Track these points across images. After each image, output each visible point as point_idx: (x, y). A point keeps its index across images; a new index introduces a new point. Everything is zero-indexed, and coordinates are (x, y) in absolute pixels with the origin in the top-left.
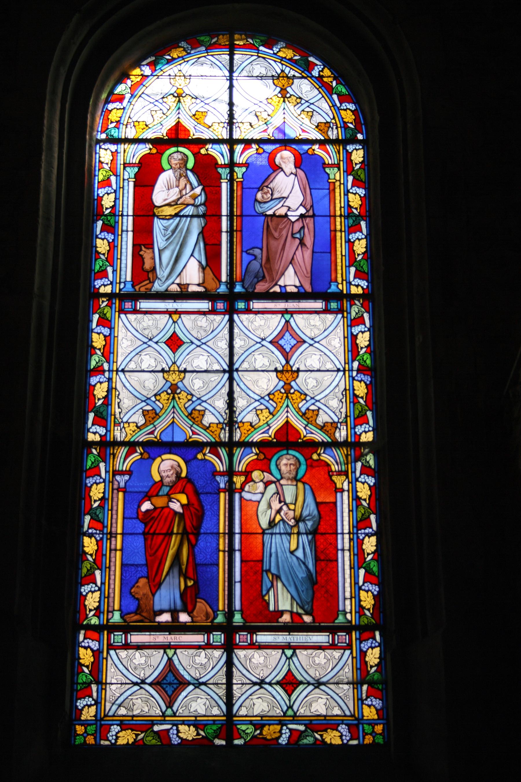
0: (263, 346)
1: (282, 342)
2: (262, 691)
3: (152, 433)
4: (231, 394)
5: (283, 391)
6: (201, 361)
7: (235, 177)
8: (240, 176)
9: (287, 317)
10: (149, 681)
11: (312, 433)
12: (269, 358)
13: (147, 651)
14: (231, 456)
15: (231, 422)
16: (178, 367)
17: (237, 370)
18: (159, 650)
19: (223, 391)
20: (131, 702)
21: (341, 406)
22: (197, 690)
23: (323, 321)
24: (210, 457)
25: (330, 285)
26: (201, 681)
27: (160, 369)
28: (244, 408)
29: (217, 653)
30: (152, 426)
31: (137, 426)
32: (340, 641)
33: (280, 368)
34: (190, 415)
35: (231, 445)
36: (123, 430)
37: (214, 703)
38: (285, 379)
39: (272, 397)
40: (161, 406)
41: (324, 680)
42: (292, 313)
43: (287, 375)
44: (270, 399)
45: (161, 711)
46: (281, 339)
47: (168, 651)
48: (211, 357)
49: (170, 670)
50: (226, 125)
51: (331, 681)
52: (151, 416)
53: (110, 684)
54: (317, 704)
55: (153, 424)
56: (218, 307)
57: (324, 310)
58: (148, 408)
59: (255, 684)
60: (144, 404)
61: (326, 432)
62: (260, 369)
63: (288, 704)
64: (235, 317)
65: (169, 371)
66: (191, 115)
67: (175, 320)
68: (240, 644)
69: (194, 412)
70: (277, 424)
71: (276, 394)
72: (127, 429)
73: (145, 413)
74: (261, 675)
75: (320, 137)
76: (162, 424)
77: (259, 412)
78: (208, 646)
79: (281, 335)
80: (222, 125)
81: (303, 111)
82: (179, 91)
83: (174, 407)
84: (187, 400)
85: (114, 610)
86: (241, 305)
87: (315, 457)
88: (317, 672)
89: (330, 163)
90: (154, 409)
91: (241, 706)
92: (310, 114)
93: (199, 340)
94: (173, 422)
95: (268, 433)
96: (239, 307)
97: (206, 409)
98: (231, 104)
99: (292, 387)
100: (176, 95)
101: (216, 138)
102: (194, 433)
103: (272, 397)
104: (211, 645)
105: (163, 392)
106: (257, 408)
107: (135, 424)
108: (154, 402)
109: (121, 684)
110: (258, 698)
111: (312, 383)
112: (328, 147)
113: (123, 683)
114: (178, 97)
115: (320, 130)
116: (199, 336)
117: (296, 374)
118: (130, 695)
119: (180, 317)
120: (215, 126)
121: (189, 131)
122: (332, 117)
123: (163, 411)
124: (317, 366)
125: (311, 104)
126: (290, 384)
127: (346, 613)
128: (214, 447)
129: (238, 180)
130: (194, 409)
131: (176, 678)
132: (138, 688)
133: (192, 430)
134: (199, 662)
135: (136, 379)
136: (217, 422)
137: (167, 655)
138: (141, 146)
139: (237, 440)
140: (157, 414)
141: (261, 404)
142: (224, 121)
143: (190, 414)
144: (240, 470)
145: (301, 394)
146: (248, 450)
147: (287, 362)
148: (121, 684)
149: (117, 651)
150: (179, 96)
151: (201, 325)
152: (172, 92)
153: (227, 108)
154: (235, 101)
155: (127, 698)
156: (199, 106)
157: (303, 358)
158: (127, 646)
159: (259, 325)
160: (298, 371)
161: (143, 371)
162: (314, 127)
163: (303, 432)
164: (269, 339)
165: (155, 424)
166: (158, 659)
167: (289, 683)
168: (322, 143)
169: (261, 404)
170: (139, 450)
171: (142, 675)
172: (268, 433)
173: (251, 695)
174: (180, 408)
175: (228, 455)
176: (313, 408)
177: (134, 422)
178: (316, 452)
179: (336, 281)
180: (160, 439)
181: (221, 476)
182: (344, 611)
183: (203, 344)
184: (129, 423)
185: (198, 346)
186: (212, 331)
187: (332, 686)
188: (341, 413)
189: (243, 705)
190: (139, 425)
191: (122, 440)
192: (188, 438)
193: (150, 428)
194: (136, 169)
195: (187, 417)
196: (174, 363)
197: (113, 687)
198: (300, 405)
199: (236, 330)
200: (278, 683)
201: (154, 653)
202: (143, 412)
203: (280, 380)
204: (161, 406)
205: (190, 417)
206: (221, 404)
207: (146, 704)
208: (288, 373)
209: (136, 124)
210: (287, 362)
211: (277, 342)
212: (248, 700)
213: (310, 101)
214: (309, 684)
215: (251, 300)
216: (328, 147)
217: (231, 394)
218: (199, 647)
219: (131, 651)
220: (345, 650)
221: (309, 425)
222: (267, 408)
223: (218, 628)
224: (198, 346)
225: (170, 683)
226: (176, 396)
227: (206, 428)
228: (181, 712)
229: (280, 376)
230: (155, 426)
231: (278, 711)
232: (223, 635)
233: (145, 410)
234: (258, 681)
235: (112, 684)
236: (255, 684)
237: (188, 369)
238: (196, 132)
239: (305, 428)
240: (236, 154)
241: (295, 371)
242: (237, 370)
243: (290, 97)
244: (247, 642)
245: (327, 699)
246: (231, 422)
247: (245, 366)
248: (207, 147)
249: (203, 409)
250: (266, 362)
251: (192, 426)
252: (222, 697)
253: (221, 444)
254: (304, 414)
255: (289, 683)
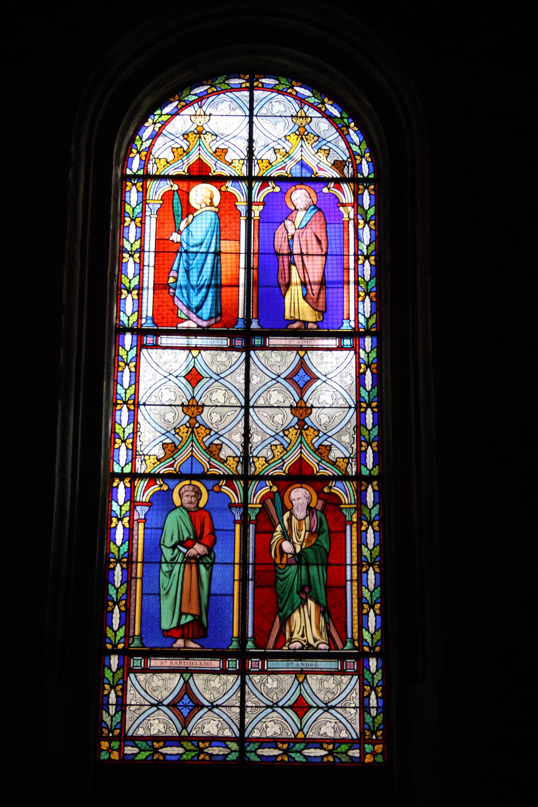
0: (278, 382)
1: (296, 378)
2: (275, 714)
3: (172, 466)
4: (247, 428)
5: (297, 427)
6: (219, 396)
7: (253, 216)
8: (257, 214)
9: (302, 353)
10: (166, 703)
11: (325, 469)
12: (281, 396)
13: (280, 676)
14: (246, 489)
15: (246, 458)
16: (305, 403)
17: (242, 407)
18: (177, 674)
19: (240, 425)
20: (264, 725)
21: (352, 442)
22: (326, 713)
23: (230, 358)
24: (226, 490)
25: (343, 323)
26: (329, 705)
27: (180, 404)
28: (259, 443)
29: (231, 678)
30: (171, 459)
31: (157, 459)
32: (230, 666)
33: (186, 403)
34: (316, 451)
35: (247, 478)
36: (144, 462)
37: (226, 726)
38: (190, 414)
39: (287, 433)
40: (289, 441)
41: (333, 704)
42: (306, 349)
43: (193, 409)
44: (285, 435)
45: (177, 731)
46: (295, 376)
47: (185, 675)
48: (229, 391)
49: (186, 693)
50: (245, 161)
51: (339, 705)
52: (171, 450)
53: (129, 705)
54: (326, 727)
55: (322, 459)
56: (345, 344)
57: (229, 347)
58: (168, 441)
59: (152, 705)
60: (164, 437)
61: (338, 467)
62: (275, 405)
63: (299, 727)
64: (252, 353)
65: (188, 406)
66: (212, 153)
67: (195, 356)
68: (252, 670)
69: (211, 445)
70: (291, 459)
71: (182, 428)
72: (257, 464)
73: (164, 446)
74: (160, 697)
75: (336, 175)
76: (181, 457)
77: (273, 448)
78: (224, 671)
79: (295, 372)
80: (242, 162)
81: (320, 148)
82: (200, 129)
83: (301, 442)
84: (205, 434)
85: (134, 635)
86: (257, 342)
87: (326, 490)
88: (212, 695)
89: (344, 202)
90: (173, 443)
91: (253, 728)
92: (327, 152)
93: (218, 375)
94: (192, 455)
95: (282, 469)
96: (256, 343)
97: (332, 444)
98: (251, 141)
99: (306, 424)
100: (196, 132)
101: (237, 175)
102: (212, 466)
103: (287, 433)
104: (227, 670)
105: (291, 427)
106: (272, 443)
107: (156, 457)
108: (282, 437)
109: (140, 705)
110: (270, 721)
111: (216, 418)
112: (342, 185)
113: (146, 705)
114: (198, 133)
115: (335, 167)
116: (219, 371)
117: (309, 410)
118: (263, 718)
119: (200, 352)
120: (236, 164)
121: (210, 168)
122: (348, 156)
123: (182, 444)
124: (222, 401)
125: (328, 142)
126: (303, 420)
127: (354, 640)
128: (230, 479)
129: (255, 218)
130: (212, 443)
131: (191, 700)
132: (271, 710)
133: (209, 464)
134: (214, 686)
135: (265, 414)
136: (235, 455)
137: (184, 679)
138: (163, 183)
139: (251, 474)
140: (176, 447)
141: (276, 439)
142: (243, 157)
143: (208, 448)
144: (144, 501)
145: (315, 430)
146: (263, 482)
147: (301, 399)
148: (140, 705)
149: (136, 674)
150: (200, 133)
151: (220, 360)
152: (193, 129)
153: (246, 144)
154: (255, 137)
155: (145, 719)
156: (219, 144)
157: (316, 396)
158: (145, 670)
159: (275, 360)
160: (312, 407)
161: (273, 407)
162: (330, 165)
163: (316, 468)
164: (283, 376)
165: (175, 457)
166: (174, 682)
167: (301, 707)
168: (337, 182)
169: (276, 439)
170: (269, 483)
171: (275, 698)
172: (282, 469)
173: (148, 716)
174: (308, 444)
175: (243, 489)
176: (326, 443)
177: (263, 457)
178: (327, 485)
179: (348, 319)
180: (179, 471)
181: (236, 508)
182: (352, 637)
183: (221, 378)
184: (258, 458)
185: (217, 381)
186: (230, 367)
187: (339, 710)
188: (353, 448)
189: (141, 726)
190: (159, 458)
191: (142, 472)
192: (206, 471)
193: (170, 461)
194: (261, 207)
195: (205, 450)
196: (193, 398)
197: (133, 708)
198: (205, 440)
199: (253, 367)
200: (290, 707)
201: (286, 677)
202: (163, 445)
203: (294, 416)
204: (289, 441)
205: (317, 453)
206: (238, 438)
207: (159, 724)
208: (302, 410)
209: (157, 161)
210: (301, 399)
211: (292, 379)
212: (146, 721)
213: (327, 139)
214: (318, 707)
215: (267, 337)
216: (240, 184)
217: (247, 428)
218: (331, 673)
219: (149, 675)
220: (353, 676)
221: (323, 462)
222: (281, 444)
223: (233, 654)
224: (217, 381)
225: (186, 704)
226: (195, 430)
227: (334, 464)
228: (311, 734)
229: (294, 412)
230: (283, 461)
231: (175, 732)
232: (238, 661)
233: (165, 443)
234: (156, 702)
235: (132, 705)
236: (152, 705)
237: (206, 404)
238: (218, 168)
239: (318, 464)
240: (254, 192)
241: (200, 406)
242: (242, 407)
243: (307, 135)
244: (258, 668)
245: (336, 723)
246: (246, 458)
247: (261, 402)
248: (227, 184)
249: (330, 444)
250: (281, 398)
251: (320, 462)
252: (234, 720)
253: (237, 477)
254: (317, 450)
255: (301, 707)
